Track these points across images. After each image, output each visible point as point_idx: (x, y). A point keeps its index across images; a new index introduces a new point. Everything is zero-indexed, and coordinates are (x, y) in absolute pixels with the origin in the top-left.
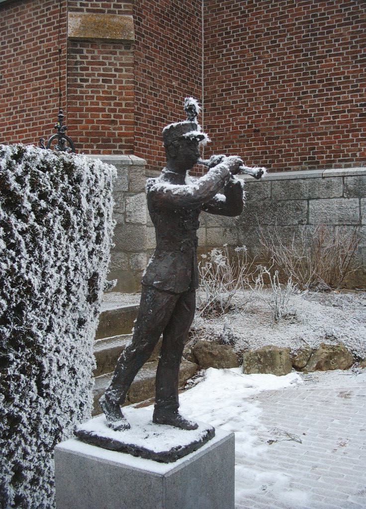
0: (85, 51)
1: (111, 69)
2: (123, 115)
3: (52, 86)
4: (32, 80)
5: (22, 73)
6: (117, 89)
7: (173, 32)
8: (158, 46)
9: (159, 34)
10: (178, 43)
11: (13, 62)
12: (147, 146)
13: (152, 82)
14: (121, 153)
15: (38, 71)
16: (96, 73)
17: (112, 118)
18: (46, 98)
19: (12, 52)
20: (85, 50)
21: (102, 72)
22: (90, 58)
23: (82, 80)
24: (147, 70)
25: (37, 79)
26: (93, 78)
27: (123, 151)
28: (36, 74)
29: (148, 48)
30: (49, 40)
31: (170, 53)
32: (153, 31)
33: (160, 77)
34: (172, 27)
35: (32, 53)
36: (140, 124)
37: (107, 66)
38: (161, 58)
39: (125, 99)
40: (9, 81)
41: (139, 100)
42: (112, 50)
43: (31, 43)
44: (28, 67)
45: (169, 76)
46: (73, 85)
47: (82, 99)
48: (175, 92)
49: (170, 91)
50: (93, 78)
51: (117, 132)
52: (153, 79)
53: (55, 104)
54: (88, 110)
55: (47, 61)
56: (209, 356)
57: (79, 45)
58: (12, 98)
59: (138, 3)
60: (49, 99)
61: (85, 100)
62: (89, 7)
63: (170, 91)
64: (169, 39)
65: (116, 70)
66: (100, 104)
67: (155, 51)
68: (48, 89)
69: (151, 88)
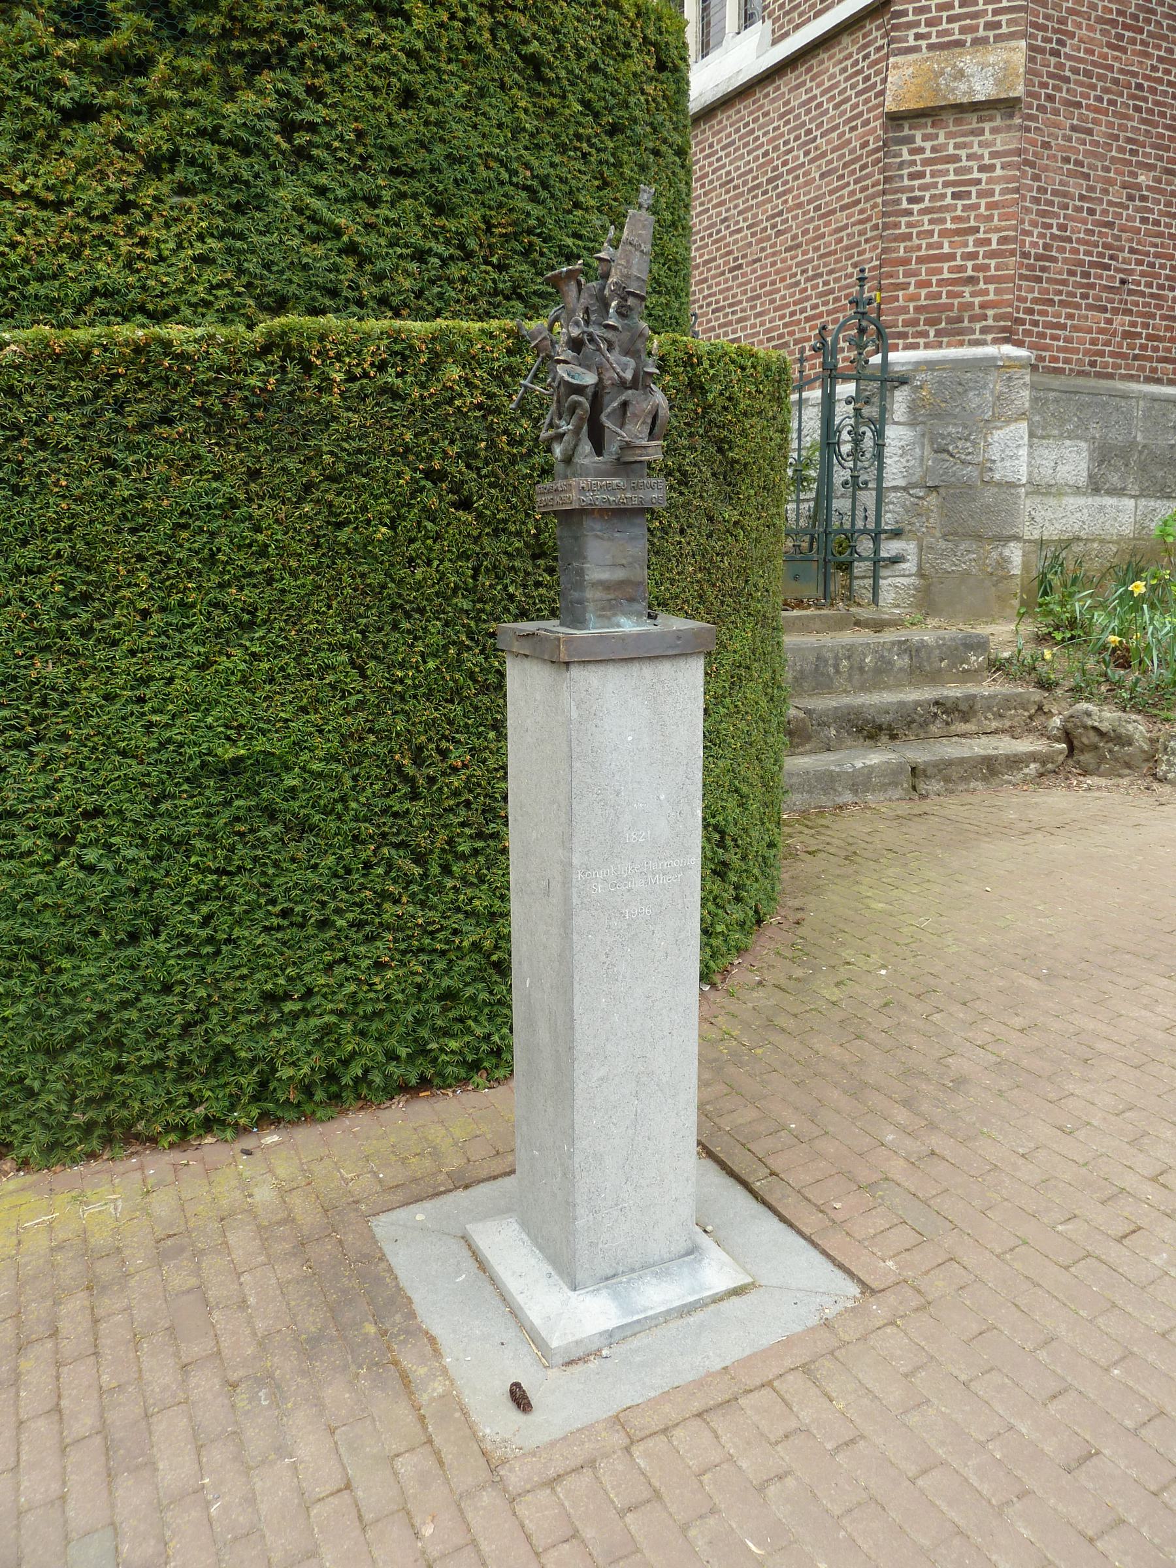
0: (918, 139)
1: (971, 168)
2: (993, 263)
3: (869, 219)
4: (833, 212)
5: (817, 198)
6: (982, 210)
7: (1147, 55)
8: (1106, 97)
9: (1110, 68)
10: (1160, 81)
11: (802, 180)
12: (1063, 327)
13: (1084, 183)
14: (982, 343)
15: (845, 191)
16: (940, 180)
17: (970, 273)
18: (858, 244)
19: (802, 159)
20: (918, 135)
21: (952, 177)
22: (928, 151)
23: (911, 200)
24: (1073, 157)
25: (843, 208)
26: (933, 191)
27: (989, 337)
28: (841, 198)
29: (1078, 105)
30: (866, 123)
31: (1138, 109)
32: (1094, 64)
33: (1107, 170)
34: (1147, 45)
35: (835, 155)
36: (1049, 280)
37: (964, 163)
38: (1110, 125)
39: (998, 230)
40: (795, 218)
41: (1050, 226)
42: (975, 125)
43: (835, 135)
44: (827, 185)
45: (1130, 163)
46: (892, 212)
47: (910, 239)
48: (1144, 198)
49: (1131, 198)
50: (933, 191)
51: (977, 300)
52: (1087, 177)
53: (874, 255)
54: (920, 260)
55: (863, 168)
56: (1092, 734)
57: (906, 126)
58: (800, 251)
59: (1057, 6)
60: (863, 246)
61: (916, 241)
62: (934, 40)
63: (1131, 198)
64: (1135, 74)
65: (982, 169)
66: (946, 245)
67: (1097, 110)
68: (861, 227)
69: (1082, 198)
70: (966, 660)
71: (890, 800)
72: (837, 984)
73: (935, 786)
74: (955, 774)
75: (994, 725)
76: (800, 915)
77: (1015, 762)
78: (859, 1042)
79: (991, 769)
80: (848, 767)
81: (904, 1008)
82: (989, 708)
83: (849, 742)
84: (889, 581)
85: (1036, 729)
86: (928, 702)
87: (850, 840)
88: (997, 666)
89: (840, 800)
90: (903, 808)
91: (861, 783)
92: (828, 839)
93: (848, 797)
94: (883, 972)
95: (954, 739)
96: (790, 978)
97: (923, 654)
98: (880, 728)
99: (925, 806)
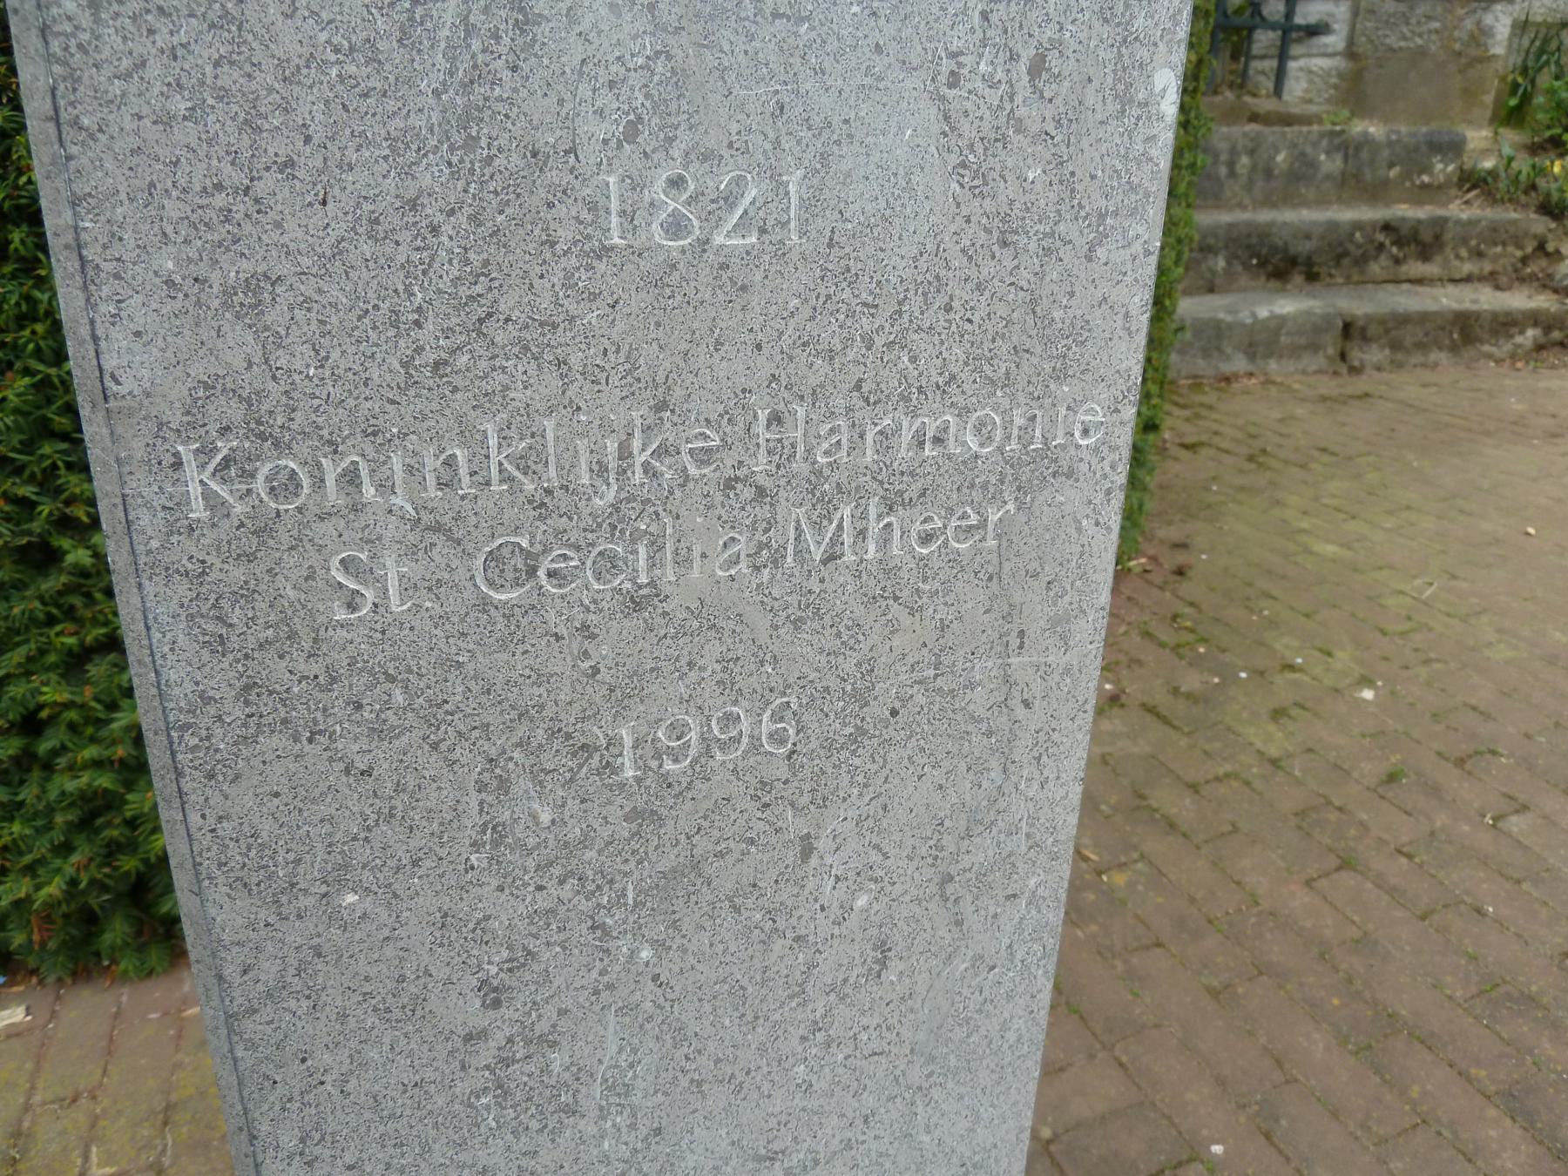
70: (1427, 169)
71: (1304, 372)
72: (1278, 714)
73: (1375, 354)
74: (1404, 337)
75: (1468, 268)
76: (1181, 558)
77: (1505, 324)
78: (1347, 879)
79: (1465, 331)
80: (1245, 316)
81: (1434, 791)
82: (1465, 241)
83: (1244, 280)
84: (1302, 62)
85: (1533, 277)
86: (1373, 225)
87: (1252, 430)
88: (1472, 181)
89: (1226, 368)
90: (1328, 386)
91: (1262, 343)
92: (1215, 427)
93: (1239, 364)
94: (1368, 694)
95: (1405, 286)
96: (1175, 691)
97: (1365, 155)
98: (1293, 262)
99: (1360, 384)
